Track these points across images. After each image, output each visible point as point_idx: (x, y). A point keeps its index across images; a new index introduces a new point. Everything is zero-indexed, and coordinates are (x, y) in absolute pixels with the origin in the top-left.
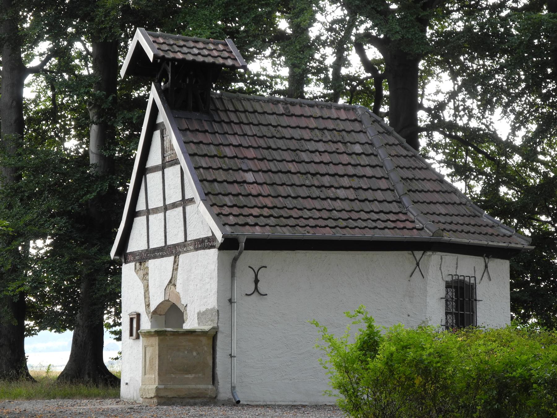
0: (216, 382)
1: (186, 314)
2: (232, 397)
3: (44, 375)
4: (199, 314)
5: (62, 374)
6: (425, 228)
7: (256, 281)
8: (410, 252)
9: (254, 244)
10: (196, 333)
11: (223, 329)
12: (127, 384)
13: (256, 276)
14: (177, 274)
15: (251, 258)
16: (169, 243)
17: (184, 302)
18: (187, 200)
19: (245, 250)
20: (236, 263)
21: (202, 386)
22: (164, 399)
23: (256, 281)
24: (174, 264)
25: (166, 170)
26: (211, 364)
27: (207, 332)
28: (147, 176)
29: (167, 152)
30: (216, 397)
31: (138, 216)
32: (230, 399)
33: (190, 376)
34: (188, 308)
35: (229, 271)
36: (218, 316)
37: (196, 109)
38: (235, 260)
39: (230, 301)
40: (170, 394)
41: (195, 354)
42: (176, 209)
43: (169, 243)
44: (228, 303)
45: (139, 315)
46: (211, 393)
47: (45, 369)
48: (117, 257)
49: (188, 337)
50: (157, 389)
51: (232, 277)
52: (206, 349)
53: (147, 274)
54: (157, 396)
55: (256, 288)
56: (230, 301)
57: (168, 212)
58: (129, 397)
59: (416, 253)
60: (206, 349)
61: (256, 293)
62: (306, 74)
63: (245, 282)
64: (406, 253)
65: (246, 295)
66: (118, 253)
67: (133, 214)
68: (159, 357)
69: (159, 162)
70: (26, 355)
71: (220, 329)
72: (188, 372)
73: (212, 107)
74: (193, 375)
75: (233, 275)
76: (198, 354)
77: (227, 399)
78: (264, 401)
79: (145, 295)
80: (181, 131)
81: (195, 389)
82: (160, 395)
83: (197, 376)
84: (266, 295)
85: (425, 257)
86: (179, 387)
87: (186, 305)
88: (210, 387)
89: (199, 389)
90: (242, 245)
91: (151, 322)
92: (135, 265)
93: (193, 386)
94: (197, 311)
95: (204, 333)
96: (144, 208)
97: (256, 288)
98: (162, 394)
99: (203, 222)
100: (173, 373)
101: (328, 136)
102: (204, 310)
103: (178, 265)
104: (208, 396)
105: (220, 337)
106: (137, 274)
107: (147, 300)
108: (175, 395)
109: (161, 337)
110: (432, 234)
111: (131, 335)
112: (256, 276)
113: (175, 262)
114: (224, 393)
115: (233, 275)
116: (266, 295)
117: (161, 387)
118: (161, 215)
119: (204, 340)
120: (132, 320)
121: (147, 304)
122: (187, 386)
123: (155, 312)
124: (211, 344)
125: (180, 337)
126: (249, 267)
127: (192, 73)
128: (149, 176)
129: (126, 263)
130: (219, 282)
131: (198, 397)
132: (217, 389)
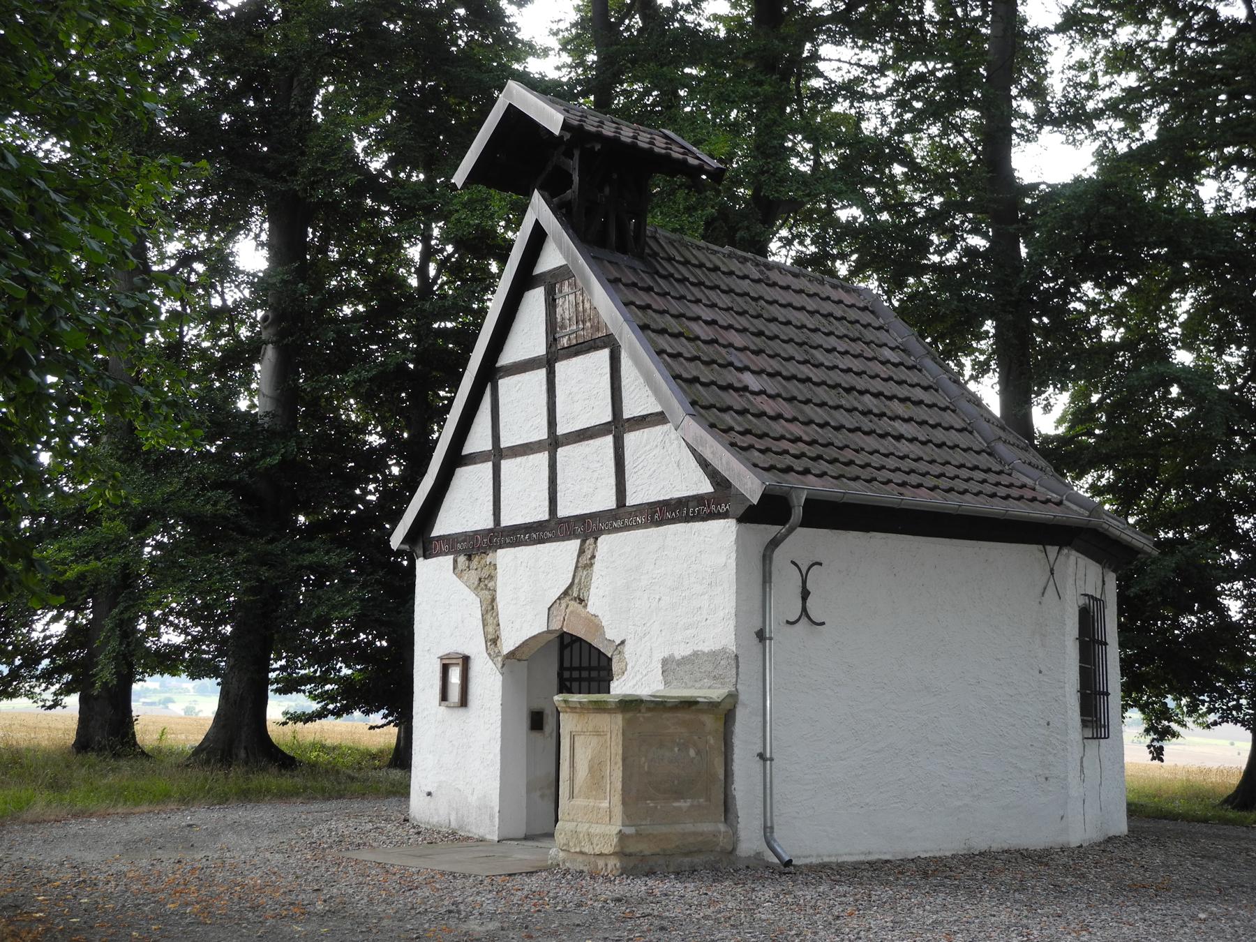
0: (731, 816)
1: (622, 660)
2: (763, 847)
3: (156, 743)
4: (665, 662)
5: (198, 750)
6: (1065, 502)
7: (805, 594)
8: (1041, 547)
9: (825, 514)
10: (699, 706)
11: (748, 696)
12: (429, 794)
13: (804, 582)
14: (589, 577)
15: (805, 542)
16: (562, 512)
17: (611, 634)
18: (628, 420)
19: (803, 525)
20: (773, 551)
21: (706, 827)
22: (636, 861)
23: (805, 594)
24: (579, 556)
25: (561, 367)
26: (722, 777)
27: (719, 703)
28: (500, 382)
29: (563, 327)
30: (734, 849)
31: (466, 465)
32: (758, 854)
33: (684, 804)
34: (628, 650)
35: (761, 570)
36: (737, 667)
37: (622, 248)
38: (774, 543)
39: (761, 636)
40: (644, 847)
41: (692, 753)
42: (591, 442)
43: (562, 512)
44: (756, 641)
45: (466, 661)
46: (723, 842)
47: (156, 736)
48: (406, 547)
49: (681, 715)
50: (622, 836)
51: (764, 582)
52: (712, 741)
53: (491, 577)
54: (621, 854)
55: (804, 610)
56: (761, 636)
57: (562, 452)
58: (435, 820)
59: (1049, 548)
60: (712, 741)
61: (804, 620)
62: (20, 530)
63: (785, 601)
64: (1034, 549)
65: (788, 622)
66: (410, 538)
67: (456, 459)
68: (624, 760)
69: (539, 348)
70: (134, 714)
71: (742, 697)
72: (679, 795)
73: (647, 251)
74: (689, 803)
75: (766, 579)
76: (698, 753)
77: (752, 853)
78: (818, 856)
79: (483, 620)
80: (612, 283)
81: (695, 834)
82: (627, 851)
83: (695, 803)
84: (823, 623)
85: (1062, 558)
86: (664, 829)
87: (623, 642)
88: (722, 827)
89: (702, 834)
90: (798, 513)
91: (502, 674)
92: (455, 561)
93: (689, 827)
94: (659, 656)
95: (712, 706)
96: (487, 445)
97: (804, 610)
98: (633, 848)
99: (667, 463)
100: (652, 799)
101: (841, 329)
102: (688, 652)
103: (593, 557)
104: (718, 849)
105: (740, 714)
106: (460, 577)
107: (490, 629)
108: (658, 850)
109: (629, 715)
110: (1087, 513)
111: (444, 697)
112: (804, 582)
113: (581, 552)
114: (750, 842)
115: (766, 579)
116: (823, 623)
117: (630, 831)
118: (542, 458)
119: (709, 721)
120: (445, 669)
121: (490, 637)
122: (679, 828)
123: (512, 655)
124: (722, 729)
125: (666, 715)
126: (793, 563)
127: (615, 176)
128: (506, 385)
129: (425, 557)
130: (738, 593)
131: (700, 851)
132: (735, 833)
